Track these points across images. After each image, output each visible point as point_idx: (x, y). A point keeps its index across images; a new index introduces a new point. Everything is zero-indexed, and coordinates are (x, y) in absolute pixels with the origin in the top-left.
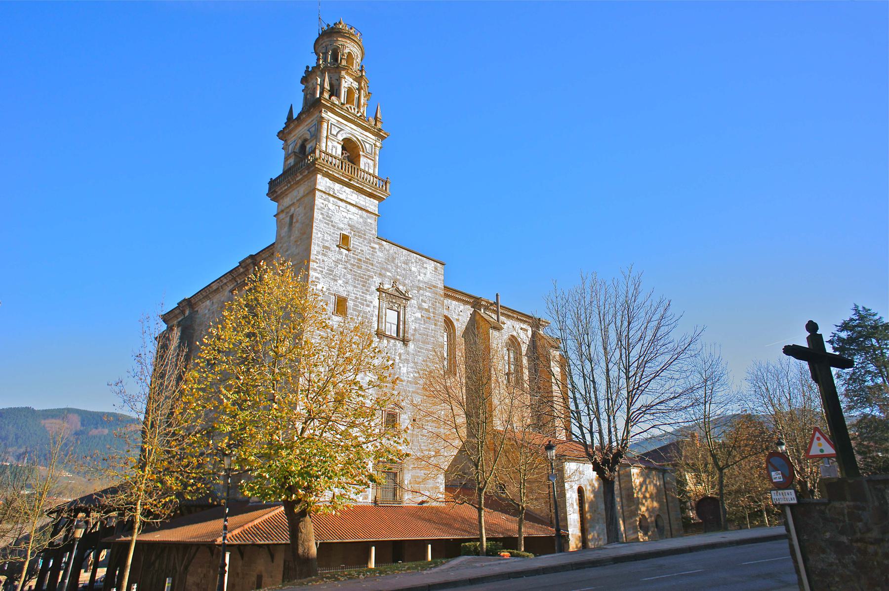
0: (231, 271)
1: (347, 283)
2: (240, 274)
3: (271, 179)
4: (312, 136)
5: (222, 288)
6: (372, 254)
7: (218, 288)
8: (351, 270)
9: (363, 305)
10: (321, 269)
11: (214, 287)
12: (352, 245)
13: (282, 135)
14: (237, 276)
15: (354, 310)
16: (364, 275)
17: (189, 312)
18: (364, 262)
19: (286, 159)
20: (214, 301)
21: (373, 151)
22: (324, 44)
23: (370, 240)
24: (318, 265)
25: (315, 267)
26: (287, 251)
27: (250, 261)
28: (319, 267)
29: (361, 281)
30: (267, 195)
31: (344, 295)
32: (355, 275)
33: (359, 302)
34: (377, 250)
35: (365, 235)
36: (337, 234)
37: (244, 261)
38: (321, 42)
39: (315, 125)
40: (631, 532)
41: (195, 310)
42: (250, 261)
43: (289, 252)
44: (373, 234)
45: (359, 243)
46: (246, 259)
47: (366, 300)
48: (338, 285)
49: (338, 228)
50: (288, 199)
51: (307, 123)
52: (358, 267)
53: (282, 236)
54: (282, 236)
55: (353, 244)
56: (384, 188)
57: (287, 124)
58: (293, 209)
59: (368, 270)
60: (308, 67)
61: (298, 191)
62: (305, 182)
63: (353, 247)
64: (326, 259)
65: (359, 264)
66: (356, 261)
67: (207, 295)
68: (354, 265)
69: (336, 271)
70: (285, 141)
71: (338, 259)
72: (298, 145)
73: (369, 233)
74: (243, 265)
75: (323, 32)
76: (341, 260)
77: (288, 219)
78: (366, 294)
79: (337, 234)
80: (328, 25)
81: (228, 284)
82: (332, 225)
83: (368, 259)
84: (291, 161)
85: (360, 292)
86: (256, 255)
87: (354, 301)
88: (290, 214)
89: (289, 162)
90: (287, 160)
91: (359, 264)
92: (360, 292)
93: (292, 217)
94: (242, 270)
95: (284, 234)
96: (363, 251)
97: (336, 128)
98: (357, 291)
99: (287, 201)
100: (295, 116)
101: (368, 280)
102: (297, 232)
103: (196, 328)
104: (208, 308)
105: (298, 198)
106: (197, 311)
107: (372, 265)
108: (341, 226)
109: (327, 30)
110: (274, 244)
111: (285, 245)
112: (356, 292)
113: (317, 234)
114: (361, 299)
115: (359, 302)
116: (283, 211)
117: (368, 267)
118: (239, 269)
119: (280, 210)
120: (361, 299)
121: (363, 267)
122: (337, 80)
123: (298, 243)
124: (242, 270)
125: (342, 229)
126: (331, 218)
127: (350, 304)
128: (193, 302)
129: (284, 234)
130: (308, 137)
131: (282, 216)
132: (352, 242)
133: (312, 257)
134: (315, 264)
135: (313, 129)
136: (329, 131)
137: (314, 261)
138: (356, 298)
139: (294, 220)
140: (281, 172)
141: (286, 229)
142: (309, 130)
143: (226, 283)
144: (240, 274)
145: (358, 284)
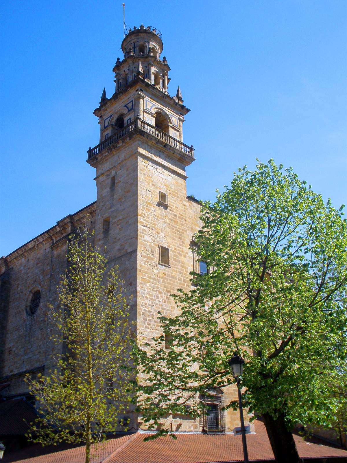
0: (48, 231)
1: (167, 235)
2: (57, 233)
3: (90, 148)
4: (129, 111)
5: (38, 246)
6: (184, 211)
7: (34, 247)
8: (169, 224)
9: (181, 255)
10: (146, 223)
11: (30, 246)
12: (168, 202)
13: (97, 112)
14: (53, 235)
15: (174, 260)
16: (179, 229)
17: (6, 270)
18: (179, 217)
19: (103, 131)
20: (30, 258)
21: (178, 123)
22: (132, 42)
23: (182, 199)
24: (144, 219)
25: (142, 220)
26: (111, 208)
27: (68, 220)
28: (145, 220)
29: (178, 234)
30: (87, 161)
31: (166, 246)
32: (173, 229)
33: (178, 253)
34: (187, 208)
35: (177, 194)
36: (156, 192)
37: (62, 221)
38: (129, 39)
39: (132, 101)
40: (77, 420)
41: (11, 267)
42: (68, 220)
43: (113, 209)
44: (183, 194)
45: (174, 201)
46: (65, 218)
47: (183, 252)
48: (161, 237)
49: (157, 188)
50: (108, 164)
51: (124, 100)
52: (175, 222)
53: (103, 195)
54: (103, 195)
55: (169, 201)
56: (190, 154)
57: (103, 103)
58: (113, 172)
59: (182, 225)
60: (118, 59)
61: (118, 156)
62: (125, 148)
63: (169, 204)
64: (149, 213)
65: (175, 219)
66: (173, 216)
67: (23, 254)
68: (171, 220)
69: (158, 225)
70: (101, 117)
71: (159, 214)
72: (115, 119)
73: (181, 193)
74: (61, 224)
75: (130, 33)
76: (161, 215)
77: (109, 181)
78: (182, 246)
79: (156, 192)
80: (135, 28)
81: (44, 243)
82: (152, 185)
83: (181, 215)
84: (109, 132)
85: (177, 243)
86: (74, 215)
87: (174, 252)
88: (112, 176)
89: (106, 133)
90: (104, 131)
91: (175, 219)
92: (177, 243)
93: (113, 179)
94: (58, 229)
95: (106, 194)
96: (177, 208)
97: (150, 104)
98: (175, 243)
99: (106, 166)
100: (109, 96)
101: (183, 233)
102: (120, 191)
103: (12, 283)
104: (24, 265)
105: (119, 162)
106: (12, 268)
107: (185, 220)
108: (159, 185)
109: (134, 30)
110: (95, 202)
111: (108, 203)
112: (175, 244)
113: (142, 191)
114: (179, 250)
115: (178, 253)
116: (102, 174)
117: (182, 222)
118: (56, 229)
119: (99, 174)
120: (179, 250)
121: (179, 222)
122: (146, 67)
123: (123, 200)
124: (58, 229)
125: (160, 188)
126: (151, 178)
127: (171, 254)
128: (9, 260)
129: (106, 194)
130: (125, 111)
131: (101, 178)
132: (168, 199)
133: (139, 212)
134: (142, 217)
135: (131, 104)
136: (145, 105)
137: (140, 215)
138: (175, 249)
139: (116, 181)
140: (98, 143)
141: (108, 189)
142: (126, 106)
143: (42, 242)
144: (57, 233)
145: (176, 236)
